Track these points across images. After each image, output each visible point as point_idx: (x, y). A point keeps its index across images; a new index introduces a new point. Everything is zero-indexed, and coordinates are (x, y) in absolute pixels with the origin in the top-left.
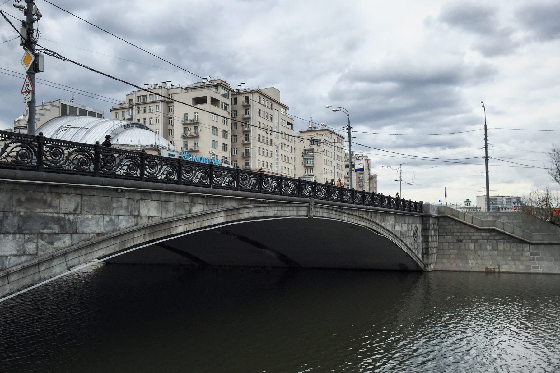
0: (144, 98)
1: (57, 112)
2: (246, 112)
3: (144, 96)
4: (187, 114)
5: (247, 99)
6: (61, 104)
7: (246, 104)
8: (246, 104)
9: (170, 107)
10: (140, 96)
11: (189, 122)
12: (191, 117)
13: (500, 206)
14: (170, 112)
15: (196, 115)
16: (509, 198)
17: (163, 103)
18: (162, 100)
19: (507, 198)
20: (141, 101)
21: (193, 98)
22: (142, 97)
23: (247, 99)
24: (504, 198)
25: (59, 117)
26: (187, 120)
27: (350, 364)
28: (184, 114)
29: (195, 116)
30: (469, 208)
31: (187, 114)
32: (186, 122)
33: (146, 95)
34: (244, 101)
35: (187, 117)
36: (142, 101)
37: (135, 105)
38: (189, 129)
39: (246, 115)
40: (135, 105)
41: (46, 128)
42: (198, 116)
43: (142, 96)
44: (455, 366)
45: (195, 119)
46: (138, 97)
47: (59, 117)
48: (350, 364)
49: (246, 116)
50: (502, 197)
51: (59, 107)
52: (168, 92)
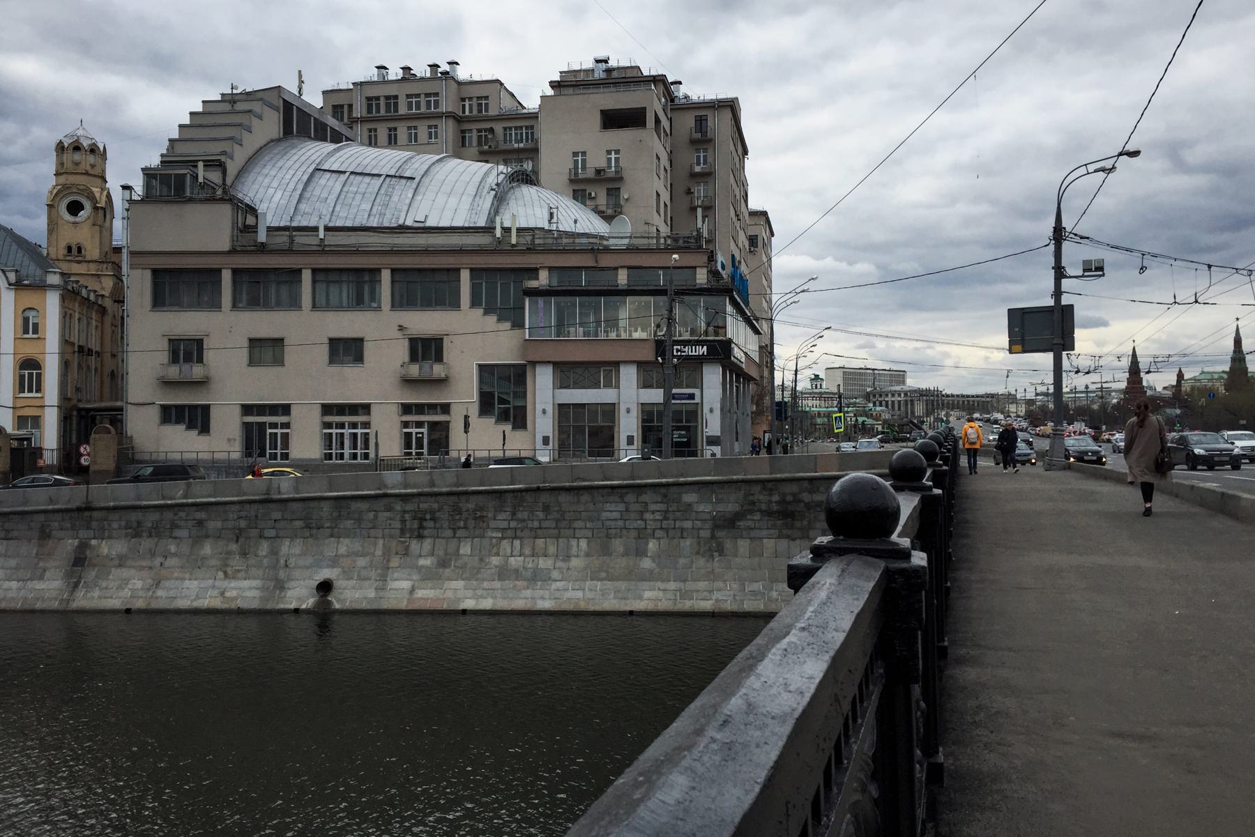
0: (388, 106)
1: (271, 125)
2: (698, 157)
3: (387, 98)
4: (584, 153)
5: (701, 122)
6: (281, 101)
7: (699, 136)
8: (699, 136)
9: (463, 132)
10: (378, 98)
11: (590, 174)
12: (596, 160)
13: (869, 390)
14: (463, 146)
15: (613, 156)
16: (886, 372)
17: (451, 123)
18: (361, 117)
19: (881, 372)
20: (378, 111)
21: (601, 111)
22: (382, 102)
23: (701, 122)
24: (876, 372)
25: (279, 140)
26: (584, 168)
27: (562, 796)
28: (575, 154)
29: (576, 162)
30: (820, 393)
31: (584, 153)
32: (580, 177)
33: (396, 97)
34: (693, 130)
35: (584, 161)
36: (383, 112)
37: (363, 120)
38: (593, 195)
39: (698, 164)
40: (363, 120)
41: (265, 171)
42: (617, 160)
43: (382, 99)
44: (189, 518)
45: (610, 167)
46: (369, 99)
47: (279, 140)
48: (562, 796)
49: (698, 169)
50: (874, 370)
51: (277, 109)
52: (459, 90)
